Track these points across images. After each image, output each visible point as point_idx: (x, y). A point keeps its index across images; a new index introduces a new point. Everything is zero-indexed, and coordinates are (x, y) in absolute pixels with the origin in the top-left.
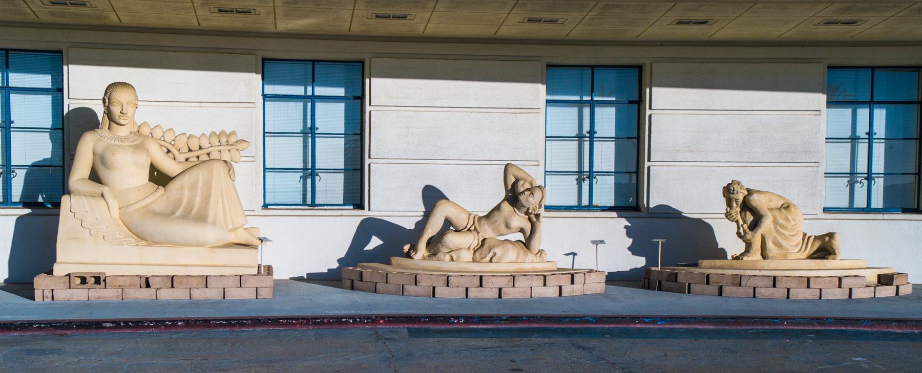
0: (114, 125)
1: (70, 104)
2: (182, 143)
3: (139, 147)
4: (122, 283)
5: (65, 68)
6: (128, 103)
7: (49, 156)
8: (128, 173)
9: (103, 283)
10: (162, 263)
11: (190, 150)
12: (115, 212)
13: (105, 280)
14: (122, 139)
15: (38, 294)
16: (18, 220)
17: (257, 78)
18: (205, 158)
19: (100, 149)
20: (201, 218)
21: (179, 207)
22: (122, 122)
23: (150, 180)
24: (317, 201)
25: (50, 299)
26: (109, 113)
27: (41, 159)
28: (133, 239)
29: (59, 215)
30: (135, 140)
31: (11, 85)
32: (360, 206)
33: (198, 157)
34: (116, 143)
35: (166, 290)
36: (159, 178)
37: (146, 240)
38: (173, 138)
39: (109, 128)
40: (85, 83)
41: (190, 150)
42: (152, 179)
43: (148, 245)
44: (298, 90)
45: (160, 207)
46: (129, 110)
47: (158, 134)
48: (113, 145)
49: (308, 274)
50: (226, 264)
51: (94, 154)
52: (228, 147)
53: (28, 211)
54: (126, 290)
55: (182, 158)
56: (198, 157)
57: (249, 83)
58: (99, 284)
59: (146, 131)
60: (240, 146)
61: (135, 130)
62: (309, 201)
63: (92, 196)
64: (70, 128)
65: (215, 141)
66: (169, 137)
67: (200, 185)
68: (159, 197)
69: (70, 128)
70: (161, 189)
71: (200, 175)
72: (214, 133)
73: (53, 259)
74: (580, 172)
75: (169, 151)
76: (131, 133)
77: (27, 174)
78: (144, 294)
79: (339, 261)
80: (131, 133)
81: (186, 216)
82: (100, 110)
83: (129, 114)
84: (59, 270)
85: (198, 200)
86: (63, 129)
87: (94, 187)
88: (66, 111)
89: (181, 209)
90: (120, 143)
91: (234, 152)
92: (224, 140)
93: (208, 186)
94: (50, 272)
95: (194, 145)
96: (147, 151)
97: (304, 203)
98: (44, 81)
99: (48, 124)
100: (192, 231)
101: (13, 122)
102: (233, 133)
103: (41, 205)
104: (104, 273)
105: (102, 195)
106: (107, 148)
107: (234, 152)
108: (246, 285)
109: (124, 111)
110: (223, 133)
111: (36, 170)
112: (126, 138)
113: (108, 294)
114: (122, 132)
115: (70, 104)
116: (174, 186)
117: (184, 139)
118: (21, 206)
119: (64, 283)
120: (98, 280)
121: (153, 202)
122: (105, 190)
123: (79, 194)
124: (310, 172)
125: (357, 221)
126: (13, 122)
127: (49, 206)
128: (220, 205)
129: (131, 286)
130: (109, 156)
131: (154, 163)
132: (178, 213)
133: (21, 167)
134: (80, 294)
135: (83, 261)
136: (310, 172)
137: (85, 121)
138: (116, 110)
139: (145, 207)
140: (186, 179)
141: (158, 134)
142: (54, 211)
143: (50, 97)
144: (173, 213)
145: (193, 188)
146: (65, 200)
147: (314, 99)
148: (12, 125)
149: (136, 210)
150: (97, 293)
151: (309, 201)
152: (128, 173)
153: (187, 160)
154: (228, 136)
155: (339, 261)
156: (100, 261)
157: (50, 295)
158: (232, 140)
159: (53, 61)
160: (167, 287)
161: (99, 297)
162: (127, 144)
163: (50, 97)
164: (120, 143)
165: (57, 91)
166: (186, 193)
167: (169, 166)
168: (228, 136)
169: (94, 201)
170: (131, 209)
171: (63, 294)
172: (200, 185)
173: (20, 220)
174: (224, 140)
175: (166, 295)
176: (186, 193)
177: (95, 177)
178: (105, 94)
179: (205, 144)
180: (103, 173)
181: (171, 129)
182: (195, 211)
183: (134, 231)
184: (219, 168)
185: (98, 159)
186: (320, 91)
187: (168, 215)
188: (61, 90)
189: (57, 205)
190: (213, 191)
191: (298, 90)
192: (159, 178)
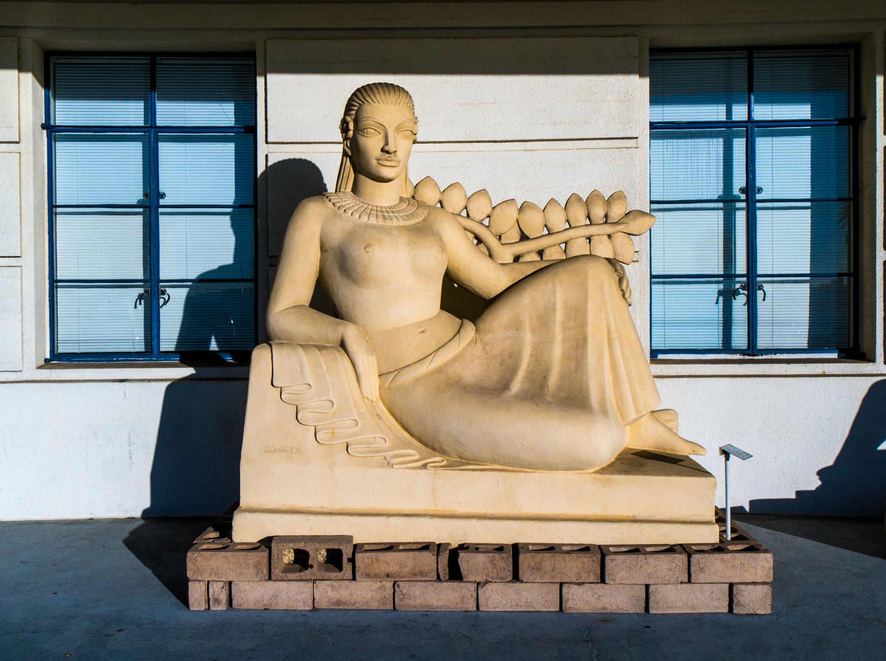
0: (367, 184)
1: (269, 155)
2: (506, 221)
3: (423, 231)
4: (393, 568)
5: (260, 81)
6: (398, 129)
7: (229, 260)
8: (400, 292)
9: (347, 567)
10: (482, 510)
11: (524, 237)
12: (372, 385)
13: (352, 560)
14: (385, 213)
15: (196, 592)
16: (169, 390)
17: (638, 86)
18: (554, 254)
19: (337, 234)
20: (574, 400)
21: (514, 371)
22: (386, 172)
23: (444, 307)
24: (762, 342)
25: (222, 607)
26: (356, 158)
27: (215, 267)
28: (414, 452)
29: (246, 379)
30: (412, 215)
31: (159, 123)
32: (855, 350)
33: (541, 253)
34: (373, 220)
35: (500, 586)
36: (463, 302)
37: (442, 452)
38: (488, 210)
39: (355, 190)
40: (301, 111)
41: (524, 237)
42: (446, 305)
43: (450, 466)
44: (715, 112)
45: (473, 370)
46: (400, 144)
47: (455, 202)
48: (367, 226)
49: (752, 503)
50: (640, 514)
51: (323, 249)
52: (608, 229)
53: (189, 371)
54: (404, 587)
55: (506, 254)
56: (541, 253)
57: (626, 97)
58: (340, 568)
59: (430, 196)
60: (634, 226)
61: (407, 195)
62: (739, 338)
63: (320, 348)
64: (270, 200)
65: (579, 215)
66: (479, 210)
67: (559, 316)
68: (468, 351)
69: (270, 200)
70: (469, 330)
71: (556, 292)
72: (574, 198)
73: (234, 504)
74: (728, 276)
75: (480, 241)
76: (402, 199)
77: (188, 299)
78: (448, 597)
79: (822, 473)
80: (402, 199)
81: (536, 395)
82: (329, 162)
83: (400, 155)
84: (246, 528)
85: (557, 351)
86: (255, 206)
87: (321, 327)
88: (261, 168)
89: (521, 374)
90: (381, 222)
91: (620, 239)
92: (598, 212)
93: (578, 316)
94: (226, 530)
95: (533, 223)
96: (438, 237)
97: (727, 346)
98: (223, 114)
99: (228, 196)
100: (557, 432)
101: (163, 196)
102: (617, 197)
103: (214, 359)
104: (349, 538)
105: (343, 345)
106: (352, 234)
107: (620, 239)
108: (702, 577)
109: (391, 147)
110: (595, 196)
111: (206, 291)
112: (391, 209)
113: (362, 593)
114: (384, 196)
115: (269, 155)
116: (499, 320)
117: (512, 213)
118: (176, 360)
119: (257, 566)
120: (334, 559)
121: (456, 359)
122: (351, 333)
123: (290, 342)
124: (739, 283)
125: (863, 386)
126: (163, 196)
127: (229, 359)
128: (607, 362)
129: (416, 576)
130: (358, 252)
131: (450, 268)
132: (516, 386)
133: (178, 283)
134: (293, 595)
135: (300, 504)
136: (739, 283)
137: (299, 181)
138: (372, 144)
139: (440, 370)
140: (527, 302)
141: (455, 202)
142: (237, 371)
143: (231, 146)
144: (505, 385)
145: (543, 322)
146: (260, 357)
147: (752, 129)
148: (162, 202)
149: (418, 380)
150: (333, 592)
151: (739, 338)
152: (400, 292)
153: (517, 259)
154: (609, 202)
155: (822, 473)
156: (338, 506)
157: (223, 597)
158: (617, 211)
159: (234, 75)
160: (502, 580)
161: (339, 602)
162: (395, 223)
163: (231, 146)
164: (381, 222)
165: (245, 133)
166: (528, 337)
167: (487, 277)
168: (609, 202)
169: (322, 358)
170: (407, 377)
171: (255, 593)
172: (559, 316)
173: (174, 389)
174: (598, 212)
175: (501, 598)
176: (528, 337)
177: (324, 301)
178: (347, 112)
179: (557, 220)
180: (343, 292)
181: (483, 192)
182: (553, 380)
183: (397, 413)
184: (599, 277)
185: (330, 257)
186: (763, 112)
187: (493, 390)
188: (253, 130)
189: (244, 359)
190: (590, 330)
191: (715, 112)
192: (463, 302)
